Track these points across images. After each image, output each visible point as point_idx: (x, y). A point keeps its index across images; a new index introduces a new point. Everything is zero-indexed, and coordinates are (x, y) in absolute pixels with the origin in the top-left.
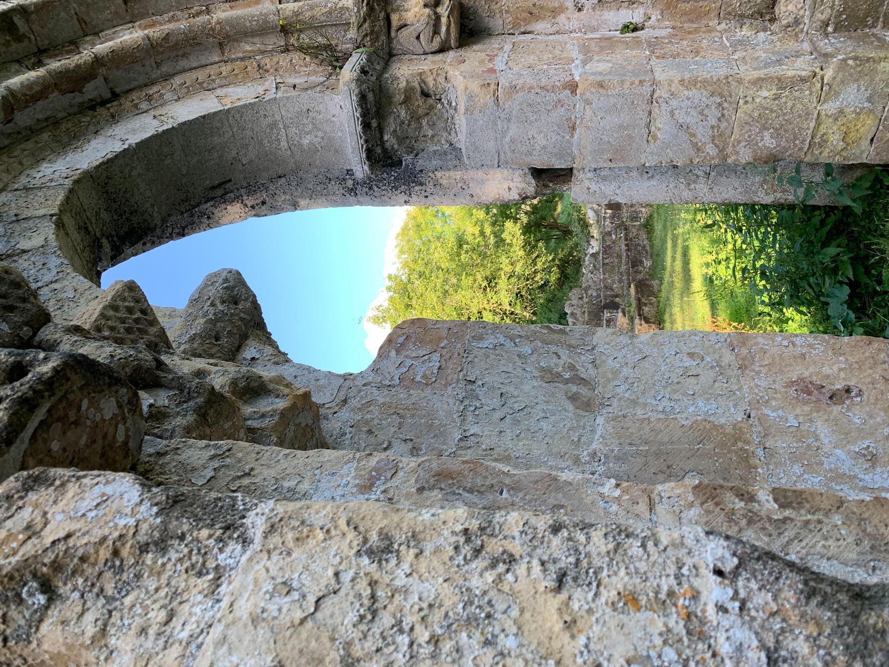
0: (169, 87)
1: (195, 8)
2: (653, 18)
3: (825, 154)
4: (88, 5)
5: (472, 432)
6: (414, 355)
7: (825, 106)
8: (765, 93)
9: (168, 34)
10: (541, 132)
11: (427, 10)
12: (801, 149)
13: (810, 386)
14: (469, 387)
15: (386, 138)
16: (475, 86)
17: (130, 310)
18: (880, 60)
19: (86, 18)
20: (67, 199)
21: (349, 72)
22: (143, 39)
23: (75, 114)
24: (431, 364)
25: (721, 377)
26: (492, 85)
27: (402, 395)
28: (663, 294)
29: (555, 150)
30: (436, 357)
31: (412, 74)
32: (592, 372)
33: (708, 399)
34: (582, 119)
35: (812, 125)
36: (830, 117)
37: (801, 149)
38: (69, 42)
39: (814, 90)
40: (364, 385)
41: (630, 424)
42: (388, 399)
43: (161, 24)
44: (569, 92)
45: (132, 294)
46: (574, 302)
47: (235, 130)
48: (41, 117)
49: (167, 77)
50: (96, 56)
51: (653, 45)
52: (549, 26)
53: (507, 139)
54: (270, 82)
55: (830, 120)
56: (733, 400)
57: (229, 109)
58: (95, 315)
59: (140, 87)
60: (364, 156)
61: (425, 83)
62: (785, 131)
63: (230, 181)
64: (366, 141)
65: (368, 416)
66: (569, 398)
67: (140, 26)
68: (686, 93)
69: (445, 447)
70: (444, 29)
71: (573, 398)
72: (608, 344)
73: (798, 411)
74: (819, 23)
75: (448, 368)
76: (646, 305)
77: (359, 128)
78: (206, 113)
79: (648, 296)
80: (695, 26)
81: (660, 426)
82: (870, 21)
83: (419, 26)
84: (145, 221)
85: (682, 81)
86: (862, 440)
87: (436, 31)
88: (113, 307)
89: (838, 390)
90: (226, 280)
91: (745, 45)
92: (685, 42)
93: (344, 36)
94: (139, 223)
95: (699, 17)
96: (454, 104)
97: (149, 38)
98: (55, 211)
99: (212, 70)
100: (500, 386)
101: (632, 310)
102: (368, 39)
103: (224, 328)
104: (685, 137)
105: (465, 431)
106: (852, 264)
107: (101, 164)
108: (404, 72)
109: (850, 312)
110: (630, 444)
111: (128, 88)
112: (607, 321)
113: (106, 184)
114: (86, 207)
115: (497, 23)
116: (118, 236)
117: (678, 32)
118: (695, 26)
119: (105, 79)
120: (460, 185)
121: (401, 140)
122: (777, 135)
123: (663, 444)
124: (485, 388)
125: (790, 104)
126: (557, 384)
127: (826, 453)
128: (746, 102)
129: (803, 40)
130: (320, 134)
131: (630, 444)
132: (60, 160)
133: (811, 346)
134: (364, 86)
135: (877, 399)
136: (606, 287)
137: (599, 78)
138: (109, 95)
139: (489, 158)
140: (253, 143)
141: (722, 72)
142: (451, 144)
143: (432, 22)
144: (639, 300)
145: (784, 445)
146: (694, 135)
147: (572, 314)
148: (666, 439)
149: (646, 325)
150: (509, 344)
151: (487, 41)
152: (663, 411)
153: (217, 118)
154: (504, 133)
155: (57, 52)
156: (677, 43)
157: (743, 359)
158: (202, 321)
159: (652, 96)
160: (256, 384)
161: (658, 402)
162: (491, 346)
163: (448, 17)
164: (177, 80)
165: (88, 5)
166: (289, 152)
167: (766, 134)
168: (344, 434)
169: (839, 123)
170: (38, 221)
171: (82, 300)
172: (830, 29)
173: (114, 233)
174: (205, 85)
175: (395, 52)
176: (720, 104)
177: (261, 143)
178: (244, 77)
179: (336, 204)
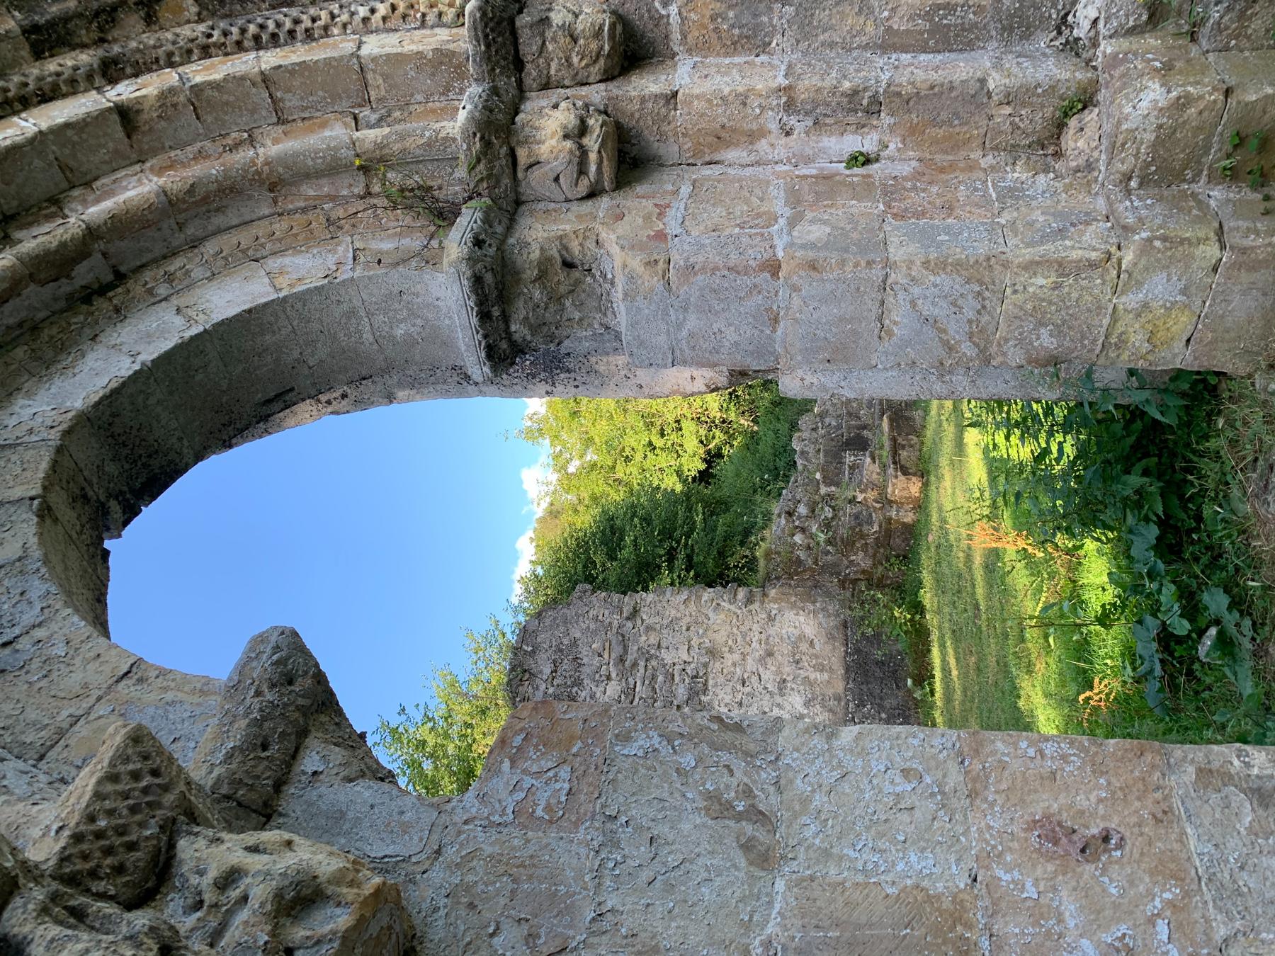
0: (197, 259)
1: (234, 135)
2: (892, 146)
3: (1125, 356)
4: (74, 147)
5: (609, 905)
6: (535, 769)
7: (1124, 299)
8: (1040, 281)
9: (192, 186)
10: (730, 325)
11: (569, 144)
12: (1092, 350)
13: (1057, 829)
14: (608, 825)
15: (513, 328)
16: (636, 263)
17: (136, 776)
18: (1199, 241)
19: (72, 163)
20: (55, 465)
21: (456, 243)
22: (158, 195)
23: (62, 311)
24: (558, 786)
25: (942, 813)
26: (661, 263)
27: (516, 842)
28: (929, 434)
29: (751, 348)
30: (564, 772)
31: (548, 238)
32: (774, 800)
33: (923, 850)
34: (788, 308)
35: (1106, 321)
36: (1130, 312)
37: (1092, 350)
38: (48, 200)
39: (1108, 278)
40: (466, 822)
41: (817, 893)
42: (497, 849)
43: (184, 165)
44: (768, 275)
45: (138, 749)
46: (806, 435)
47: (295, 323)
48: (11, 321)
49: (195, 244)
50: (88, 228)
51: (891, 190)
52: (745, 154)
53: (684, 333)
54: (343, 250)
55: (1131, 316)
56: (956, 852)
57: (285, 297)
58: (87, 797)
59: (155, 262)
60: (483, 355)
61: (567, 249)
62: (1070, 328)
63: (292, 389)
64: (485, 336)
65: (470, 878)
66: (741, 846)
67: (152, 169)
68: (932, 278)
69: (571, 933)
70: (593, 168)
71: (747, 846)
72: (797, 750)
73: (1039, 871)
74: (1118, 176)
75: (580, 791)
76: (903, 447)
77: (475, 321)
78: (252, 305)
79: (907, 434)
80: (951, 158)
81: (857, 896)
82: (1189, 174)
83: (557, 165)
84: (171, 462)
85: (926, 264)
86: (1117, 923)
87: (582, 171)
88: (113, 777)
89: (1093, 836)
90: (277, 648)
91: (1018, 198)
92: (934, 189)
93: (451, 174)
94: (162, 467)
95: (956, 147)
96: (609, 276)
97: (165, 193)
98: (36, 490)
99: (260, 229)
100: (651, 824)
101: (885, 454)
102: (485, 185)
103: (274, 730)
104: (929, 332)
105: (600, 904)
106: (1162, 495)
107: (102, 399)
108: (537, 234)
109: (1159, 561)
110: (817, 927)
111: (138, 263)
112: (850, 467)
113: (110, 424)
114: (82, 465)
115: (670, 151)
116: (132, 491)
117: (930, 171)
118: (951, 158)
119: (104, 254)
120: (623, 373)
121: (535, 329)
122: (1058, 332)
123: (859, 927)
124: (630, 829)
125: (1074, 295)
126: (727, 822)
127: (1069, 945)
128: (1015, 292)
129: (1097, 193)
130: (419, 322)
131: (817, 927)
132: (42, 392)
133: (1064, 758)
134: (479, 266)
135: (1142, 854)
136: (850, 414)
137: (811, 255)
138: (110, 277)
139: (660, 356)
140: (322, 337)
141: (982, 249)
142: (607, 328)
143: (576, 160)
144: (894, 440)
145: (1017, 931)
146: (945, 331)
147: (802, 452)
148: (863, 919)
149: (902, 478)
150: (665, 750)
151: (656, 176)
152: (864, 870)
153: (269, 311)
154: (679, 326)
155: (30, 219)
156: (924, 190)
157: (974, 780)
158: (243, 723)
159: (884, 281)
160: (309, 891)
161: (858, 855)
162: (640, 753)
163: (599, 152)
164: (210, 248)
165: (74, 147)
166: (375, 347)
167: (1042, 331)
168: (436, 910)
169: (1143, 320)
170: (13, 510)
171: (78, 661)
172: (1133, 184)
173: (125, 489)
174: (250, 253)
175: (524, 198)
176: (979, 293)
177: (334, 338)
178: (307, 239)
179: (447, 394)
